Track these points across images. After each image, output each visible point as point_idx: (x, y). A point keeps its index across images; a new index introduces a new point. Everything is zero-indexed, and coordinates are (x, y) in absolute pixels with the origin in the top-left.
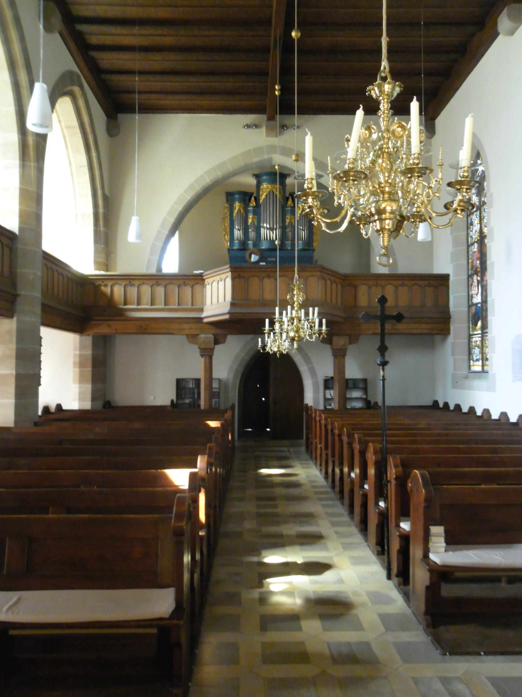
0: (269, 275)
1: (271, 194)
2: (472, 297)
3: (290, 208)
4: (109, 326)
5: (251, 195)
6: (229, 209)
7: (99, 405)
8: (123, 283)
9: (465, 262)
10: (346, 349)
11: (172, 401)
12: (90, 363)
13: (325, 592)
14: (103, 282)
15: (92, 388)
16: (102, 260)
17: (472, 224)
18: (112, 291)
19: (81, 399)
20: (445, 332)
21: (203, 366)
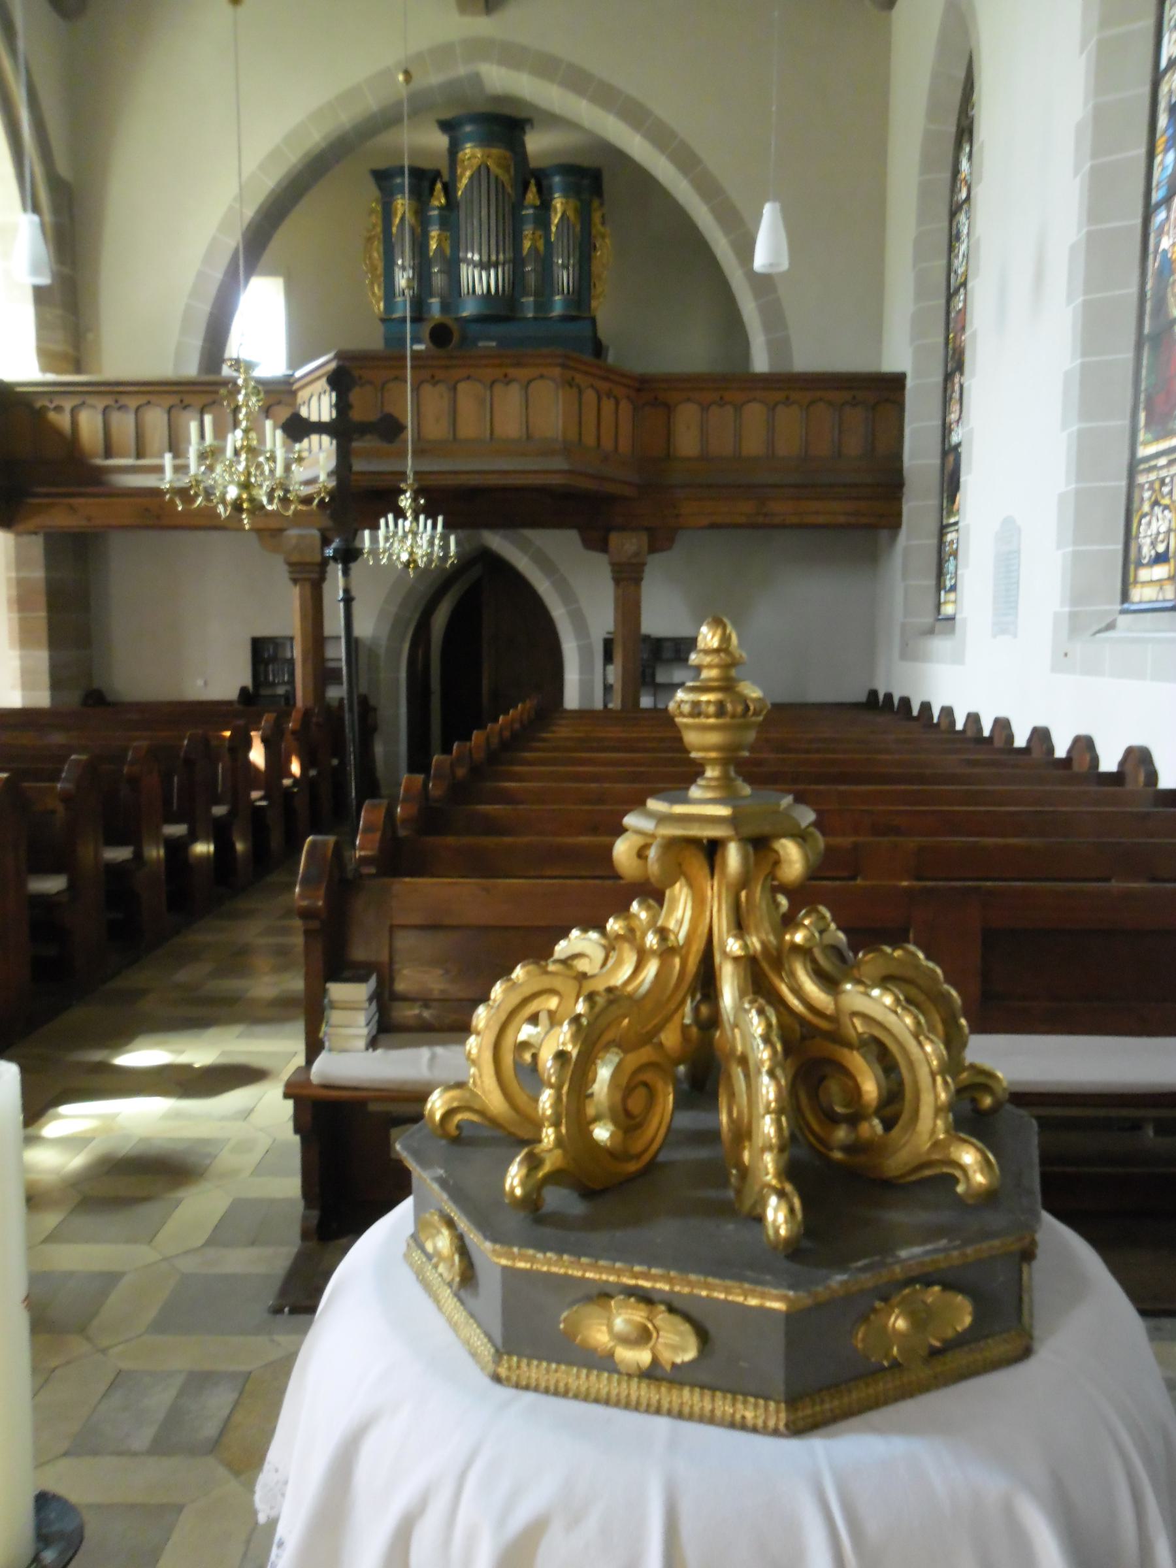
0: (433, 377)
1: (482, 171)
2: (951, 431)
3: (531, 211)
4: (72, 509)
5: (437, 175)
6: (380, 215)
7: (73, 698)
8: (100, 403)
9: (941, 340)
10: (644, 564)
11: (244, 690)
12: (42, 600)
13: (170, 1139)
14: (51, 402)
15: (51, 658)
16: (60, 345)
17: (958, 238)
18: (75, 424)
19: (27, 684)
20: (893, 522)
21: (297, 604)
